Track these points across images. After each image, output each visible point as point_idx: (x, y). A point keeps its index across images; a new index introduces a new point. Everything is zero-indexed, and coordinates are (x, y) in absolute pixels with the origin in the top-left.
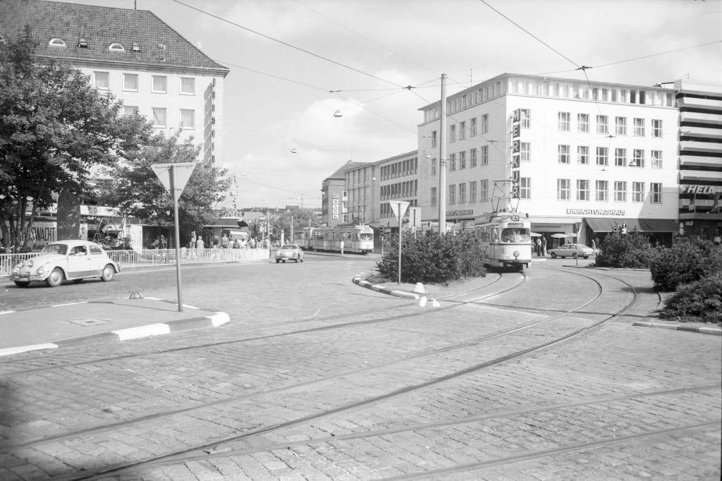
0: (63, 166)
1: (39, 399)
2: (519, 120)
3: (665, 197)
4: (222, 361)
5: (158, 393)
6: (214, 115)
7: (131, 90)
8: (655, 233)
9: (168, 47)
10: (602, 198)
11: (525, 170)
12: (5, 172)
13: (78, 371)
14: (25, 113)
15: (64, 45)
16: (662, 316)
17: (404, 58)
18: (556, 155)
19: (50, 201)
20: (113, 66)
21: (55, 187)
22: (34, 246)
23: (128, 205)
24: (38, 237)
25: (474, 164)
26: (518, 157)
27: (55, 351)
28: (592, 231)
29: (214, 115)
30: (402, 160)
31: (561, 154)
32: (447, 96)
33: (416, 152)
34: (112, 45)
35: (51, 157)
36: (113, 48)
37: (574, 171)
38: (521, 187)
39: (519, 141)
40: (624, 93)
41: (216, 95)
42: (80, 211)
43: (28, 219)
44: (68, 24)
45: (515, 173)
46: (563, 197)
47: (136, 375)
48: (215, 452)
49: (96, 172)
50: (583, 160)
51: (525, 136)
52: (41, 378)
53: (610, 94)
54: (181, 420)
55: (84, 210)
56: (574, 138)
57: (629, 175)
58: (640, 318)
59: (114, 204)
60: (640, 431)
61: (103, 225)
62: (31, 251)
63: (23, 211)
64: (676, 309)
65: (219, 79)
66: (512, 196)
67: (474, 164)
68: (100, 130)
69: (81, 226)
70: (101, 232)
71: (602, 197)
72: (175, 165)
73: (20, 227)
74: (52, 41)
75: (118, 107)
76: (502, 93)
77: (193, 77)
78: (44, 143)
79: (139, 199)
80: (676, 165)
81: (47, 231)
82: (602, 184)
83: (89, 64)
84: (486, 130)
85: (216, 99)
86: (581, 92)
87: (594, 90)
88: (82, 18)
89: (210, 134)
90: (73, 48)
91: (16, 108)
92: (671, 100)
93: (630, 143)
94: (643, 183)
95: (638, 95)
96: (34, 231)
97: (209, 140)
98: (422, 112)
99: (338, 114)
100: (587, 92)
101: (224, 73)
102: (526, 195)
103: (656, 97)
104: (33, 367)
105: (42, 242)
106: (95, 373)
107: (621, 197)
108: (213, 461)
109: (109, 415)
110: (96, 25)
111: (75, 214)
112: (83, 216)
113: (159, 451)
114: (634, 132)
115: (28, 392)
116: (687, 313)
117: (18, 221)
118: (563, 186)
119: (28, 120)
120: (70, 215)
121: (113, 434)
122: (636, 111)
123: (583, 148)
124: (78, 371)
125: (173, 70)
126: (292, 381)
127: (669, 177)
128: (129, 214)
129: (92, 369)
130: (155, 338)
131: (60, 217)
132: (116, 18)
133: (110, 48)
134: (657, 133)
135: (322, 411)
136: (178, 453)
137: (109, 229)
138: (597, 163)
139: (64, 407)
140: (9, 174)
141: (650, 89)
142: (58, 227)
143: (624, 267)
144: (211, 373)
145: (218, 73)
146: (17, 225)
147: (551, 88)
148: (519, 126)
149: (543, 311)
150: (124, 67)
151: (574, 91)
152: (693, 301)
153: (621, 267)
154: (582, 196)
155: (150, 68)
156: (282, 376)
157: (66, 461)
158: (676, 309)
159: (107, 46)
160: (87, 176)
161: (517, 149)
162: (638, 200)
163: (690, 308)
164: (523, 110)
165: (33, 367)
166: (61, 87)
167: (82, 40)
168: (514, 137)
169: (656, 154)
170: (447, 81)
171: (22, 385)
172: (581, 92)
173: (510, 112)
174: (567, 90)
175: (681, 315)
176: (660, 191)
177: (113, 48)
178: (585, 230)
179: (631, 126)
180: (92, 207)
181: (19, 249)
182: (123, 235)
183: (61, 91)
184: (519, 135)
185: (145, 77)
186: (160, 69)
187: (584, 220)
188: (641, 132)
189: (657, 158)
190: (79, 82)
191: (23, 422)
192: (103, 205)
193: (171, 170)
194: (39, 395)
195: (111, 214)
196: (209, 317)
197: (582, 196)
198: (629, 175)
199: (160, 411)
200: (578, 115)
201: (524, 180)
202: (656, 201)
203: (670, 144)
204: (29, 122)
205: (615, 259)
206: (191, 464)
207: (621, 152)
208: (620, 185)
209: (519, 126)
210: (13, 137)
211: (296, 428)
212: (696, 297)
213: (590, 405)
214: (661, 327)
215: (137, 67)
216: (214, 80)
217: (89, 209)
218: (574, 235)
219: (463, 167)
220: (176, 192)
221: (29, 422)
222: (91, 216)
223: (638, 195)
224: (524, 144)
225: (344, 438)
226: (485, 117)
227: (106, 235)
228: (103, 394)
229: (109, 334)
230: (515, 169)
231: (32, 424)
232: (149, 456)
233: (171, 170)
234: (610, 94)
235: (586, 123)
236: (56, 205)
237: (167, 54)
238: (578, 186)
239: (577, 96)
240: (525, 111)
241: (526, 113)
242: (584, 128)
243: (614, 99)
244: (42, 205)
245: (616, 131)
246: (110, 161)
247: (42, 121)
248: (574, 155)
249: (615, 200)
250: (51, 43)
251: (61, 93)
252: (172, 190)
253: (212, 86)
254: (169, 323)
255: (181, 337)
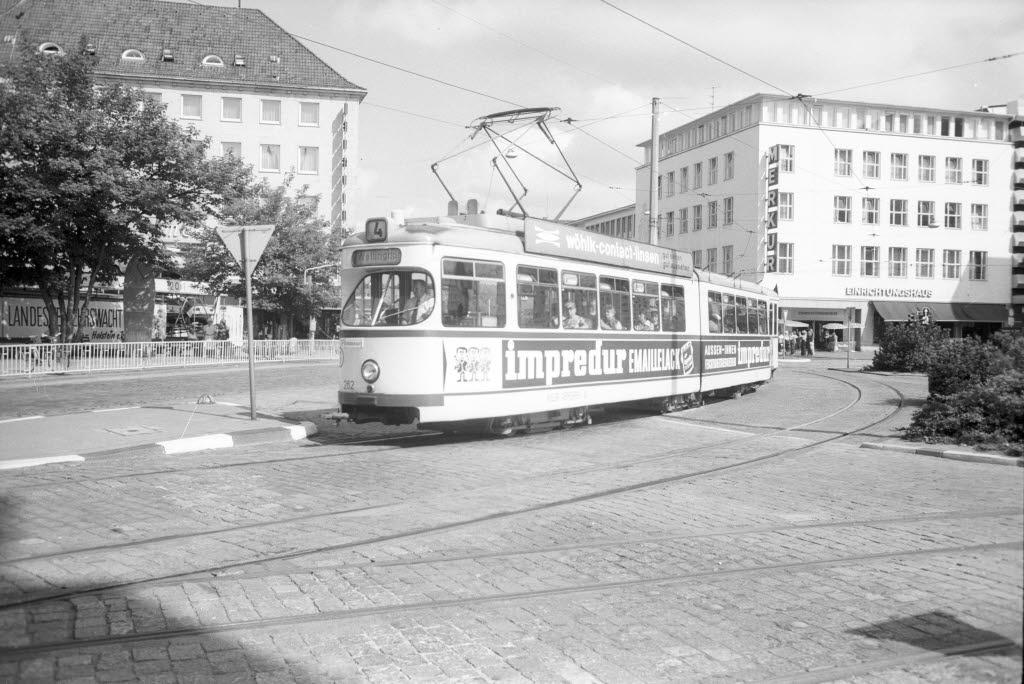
0: (131, 226)
1: (39, 516)
2: (777, 161)
3: (990, 271)
4: (281, 480)
5: (187, 513)
6: (346, 154)
7: (230, 120)
8: (976, 323)
9: (284, 60)
10: (898, 273)
11: (785, 232)
12: (51, 234)
13: (97, 486)
14: (81, 155)
15: (142, 58)
16: (909, 436)
17: (627, 69)
18: (831, 210)
19: (116, 271)
20: (207, 86)
21: (121, 255)
22: (94, 334)
23: (221, 278)
24: (100, 322)
25: (713, 224)
26: (776, 213)
27: (79, 464)
28: (882, 319)
29: (346, 154)
30: (615, 217)
31: (838, 209)
32: (660, 134)
33: (632, 207)
34: (207, 58)
35: (114, 215)
36: (208, 61)
37: (857, 235)
38: (780, 258)
39: (776, 191)
40: (931, 121)
41: (349, 126)
42: (154, 288)
43: (83, 297)
44: (147, 29)
45: (770, 236)
46: (841, 271)
47: (165, 492)
48: (224, 574)
49: (174, 234)
50: (871, 218)
51: (783, 186)
52: (48, 494)
53: (911, 122)
54: (197, 543)
55: (161, 285)
56: (854, 187)
57: (940, 239)
58: (876, 438)
59: (204, 277)
60: (753, 565)
61: (188, 307)
62: (88, 341)
63: (77, 288)
64: (924, 427)
65: (353, 105)
66: (766, 268)
67: (713, 224)
68: (179, 176)
69: (157, 307)
70: (186, 315)
71: (897, 271)
72: (246, 228)
73: (72, 308)
74: (126, 52)
75: (205, 146)
76: (753, 121)
77: (317, 101)
78: (102, 196)
79: (234, 271)
80: (1007, 225)
81: (111, 313)
82: (899, 252)
83: (175, 84)
84: (730, 175)
85: (348, 133)
86: (869, 120)
87: (887, 117)
88: (166, 21)
89: (339, 181)
90: (153, 62)
91: (67, 148)
92: (1002, 131)
93: (940, 193)
94: (958, 252)
95: (953, 124)
96: (93, 313)
97: (338, 189)
98: (643, 148)
99: (511, 154)
100: (878, 122)
101: (360, 96)
102: (786, 268)
103: (980, 126)
104: (45, 482)
105: (105, 329)
106: (117, 489)
107: (925, 271)
108: (215, 583)
109: (118, 535)
110: (186, 29)
111: (148, 291)
112: (160, 294)
113: (156, 572)
114: (947, 178)
115: (28, 508)
116: (938, 431)
117: (69, 299)
118: (841, 255)
119: (82, 164)
120: (142, 293)
121: (114, 555)
122: (950, 147)
123: (843, 199)
124: (97, 486)
125: (289, 92)
126: (360, 503)
127: (998, 244)
128: (221, 292)
129: (116, 484)
130: (212, 451)
131: (128, 295)
132: (214, 20)
133: (204, 61)
134: (980, 180)
135: (376, 537)
136: (180, 575)
137: (197, 312)
138: (891, 222)
139: (66, 525)
140: (56, 236)
141: (970, 115)
142: (125, 308)
143: (912, 371)
144: (259, 492)
145: (352, 96)
146: (69, 305)
147: (839, 116)
148: (777, 169)
149: (749, 428)
150: (223, 88)
151: (858, 118)
152: (946, 416)
153: (907, 371)
154: (869, 270)
155: (258, 89)
156: (349, 497)
157: (47, 579)
158: (924, 427)
159: (200, 59)
160: (162, 239)
161: (773, 203)
162: (951, 275)
163: (941, 425)
164: (783, 147)
165: (45, 482)
166: (128, 119)
167: (166, 51)
168: (770, 185)
169: (979, 209)
170: (660, 108)
171: (24, 501)
172: (869, 120)
173: (764, 148)
174: (848, 117)
175: (929, 434)
176: (984, 263)
177: (208, 61)
178: (872, 318)
179: (941, 169)
180: (173, 281)
181: (71, 337)
182: (216, 320)
183: (126, 125)
184: (776, 183)
185: (252, 102)
186: (272, 90)
187: (871, 304)
188: (956, 178)
189: (980, 215)
190: (153, 112)
191: (13, 539)
192: (188, 279)
193: (242, 235)
194: (40, 511)
195: (196, 291)
196: (288, 428)
197: (869, 270)
198: (940, 239)
199: (180, 532)
200: (892, 156)
201: (783, 246)
202: (978, 276)
203: (999, 195)
204: (83, 166)
205: (900, 359)
206: (187, 585)
207: (926, 205)
208: (925, 254)
209: (777, 169)
210: (62, 187)
211: (333, 553)
212: (951, 410)
213: (700, 539)
214: (896, 450)
215: (240, 88)
216: (346, 105)
217: (169, 284)
218: (856, 326)
219: (699, 227)
220: (248, 264)
221: (20, 539)
222: (172, 294)
223: (951, 268)
224: (784, 195)
225: (383, 565)
226: (730, 156)
227: (192, 320)
228: (119, 513)
229: (152, 446)
230: (772, 231)
231: (22, 542)
232: (145, 577)
233: (242, 235)
234: (911, 122)
235: (875, 165)
236: (121, 279)
237: (282, 70)
238: (862, 256)
239: (863, 127)
240: (786, 147)
241: (787, 150)
242: (900, 174)
243: (917, 129)
244: (102, 279)
245: (920, 177)
246: (194, 219)
247: (100, 165)
248: (858, 211)
249: (917, 275)
250: (124, 56)
251: (127, 127)
252: (244, 261)
253: (343, 114)
254: (232, 434)
255: (246, 452)
